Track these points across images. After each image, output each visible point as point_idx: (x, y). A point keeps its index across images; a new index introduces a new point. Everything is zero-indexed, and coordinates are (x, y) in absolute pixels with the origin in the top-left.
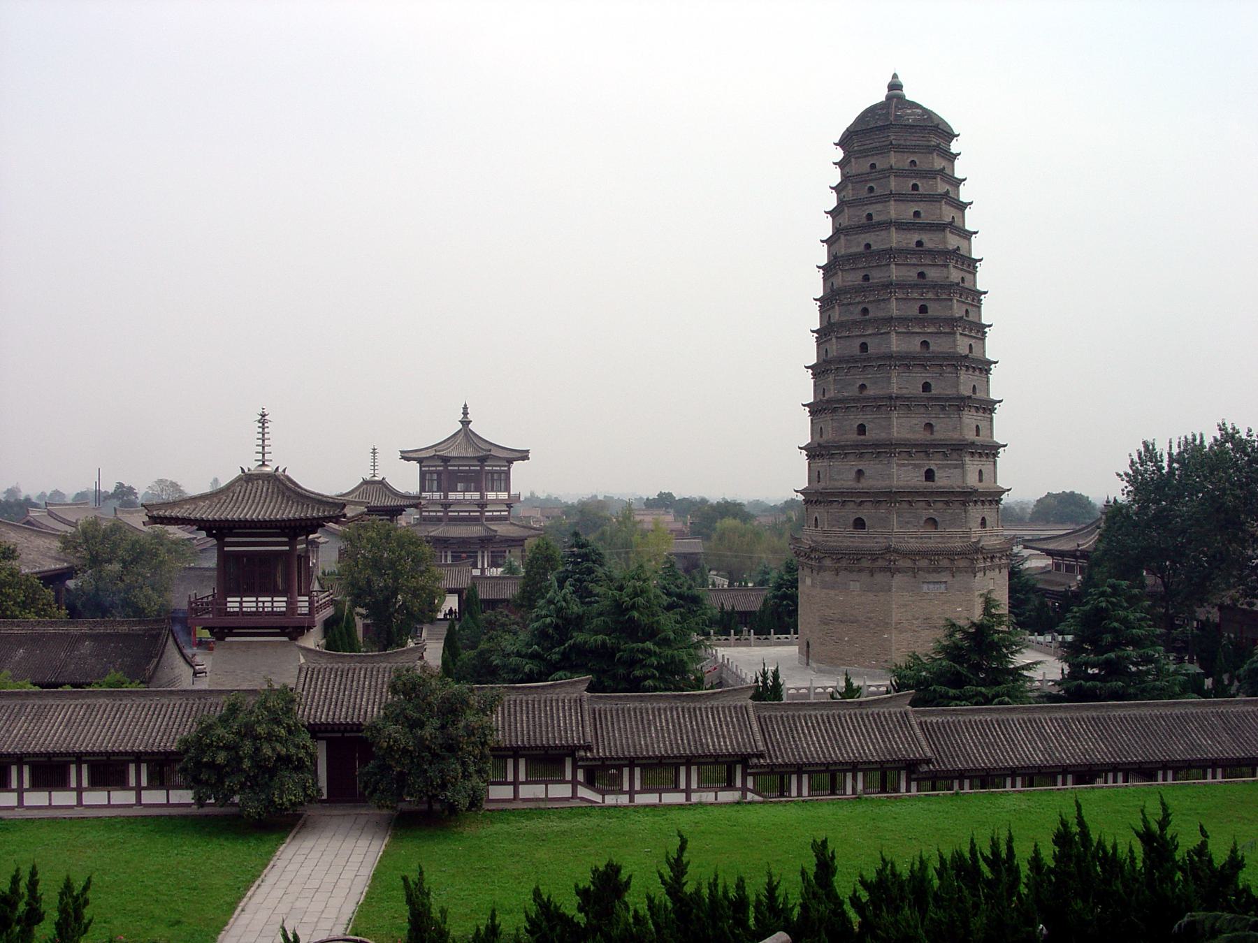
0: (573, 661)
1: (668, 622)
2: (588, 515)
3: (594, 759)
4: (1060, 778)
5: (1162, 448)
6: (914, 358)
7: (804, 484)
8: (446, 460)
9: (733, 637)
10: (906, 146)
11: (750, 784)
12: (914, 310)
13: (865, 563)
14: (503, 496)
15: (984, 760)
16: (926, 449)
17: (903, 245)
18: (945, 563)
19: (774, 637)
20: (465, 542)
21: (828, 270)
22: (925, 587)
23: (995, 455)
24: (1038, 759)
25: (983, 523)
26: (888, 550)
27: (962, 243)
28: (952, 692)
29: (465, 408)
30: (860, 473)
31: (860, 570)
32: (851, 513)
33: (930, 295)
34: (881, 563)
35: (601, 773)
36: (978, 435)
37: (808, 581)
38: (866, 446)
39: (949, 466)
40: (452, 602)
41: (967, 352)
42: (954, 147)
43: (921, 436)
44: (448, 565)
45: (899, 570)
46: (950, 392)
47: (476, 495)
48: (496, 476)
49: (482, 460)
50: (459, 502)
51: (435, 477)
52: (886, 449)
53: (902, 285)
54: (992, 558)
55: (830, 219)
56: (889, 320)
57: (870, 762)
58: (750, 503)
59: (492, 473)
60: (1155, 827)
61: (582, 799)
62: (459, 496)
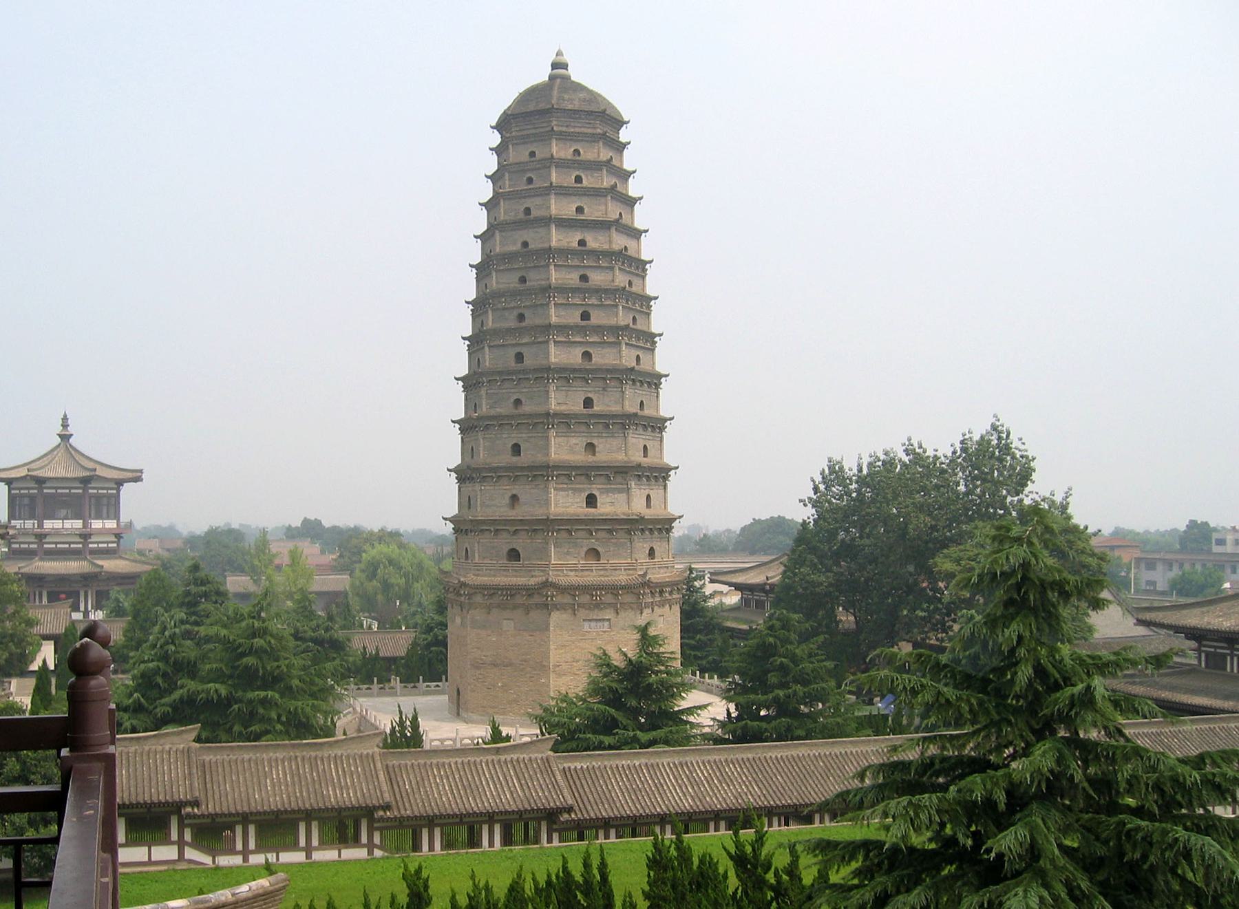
0: (181, 714)
1: (294, 663)
2: (225, 547)
3: (203, 816)
4: (712, 825)
5: (850, 468)
6: (574, 370)
7: (453, 510)
8: (40, 481)
9: (375, 686)
10: (569, 134)
11: (377, 840)
12: (574, 318)
13: (519, 600)
14: (111, 524)
15: (628, 807)
16: (586, 472)
17: (564, 244)
18: (609, 598)
19: (422, 685)
20: (62, 579)
21: (482, 270)
22: (586, 624)
23: (665, 478)
24: (687, 804)
25: (652, 553)
26: (546, 584)
27: (631, 244)
28: (607, 740)
29: (65, 419)
30: (514, 498)
31: (515, 607)
32: (504, 543)
33: (594, 301)
34: (537, 599)
35: (212, 831)
36: (645, 455)
37: (458, 620)
38: (522, 468)
39: (613, 491)
40: (47, 654)
41: (634, 364)
42: (623, 136)
43: (580, 457)
44: (45, 607)
45: (556, 607)
46: (615, 409)
47: (78, 524)
48: (105, 501)
49: (85, 481)
50: (56, 532)
51: (26, 501)
52: (543, 472)
53: (563, 290)
54: (661, 592)
55: (485, 211)
56: (548, 328)
57: (506, 812)
58: (415, 533)
59: (98, 498)
60: (749, 849)
61: (190, 861)
62: (57, 524)
